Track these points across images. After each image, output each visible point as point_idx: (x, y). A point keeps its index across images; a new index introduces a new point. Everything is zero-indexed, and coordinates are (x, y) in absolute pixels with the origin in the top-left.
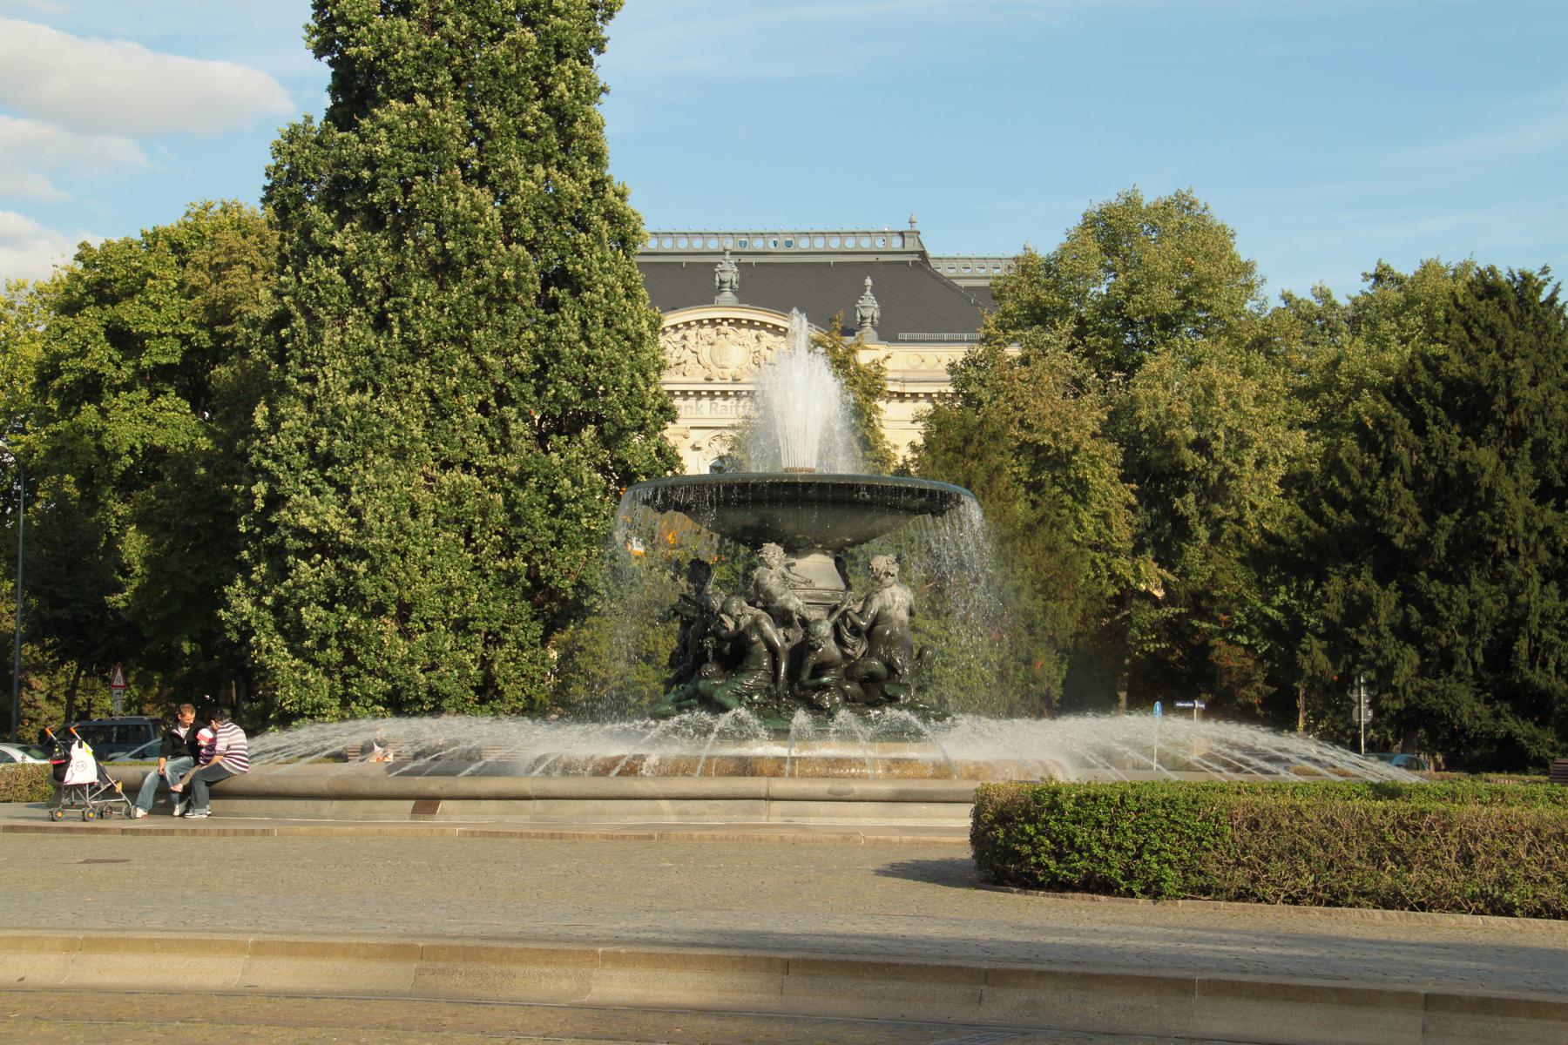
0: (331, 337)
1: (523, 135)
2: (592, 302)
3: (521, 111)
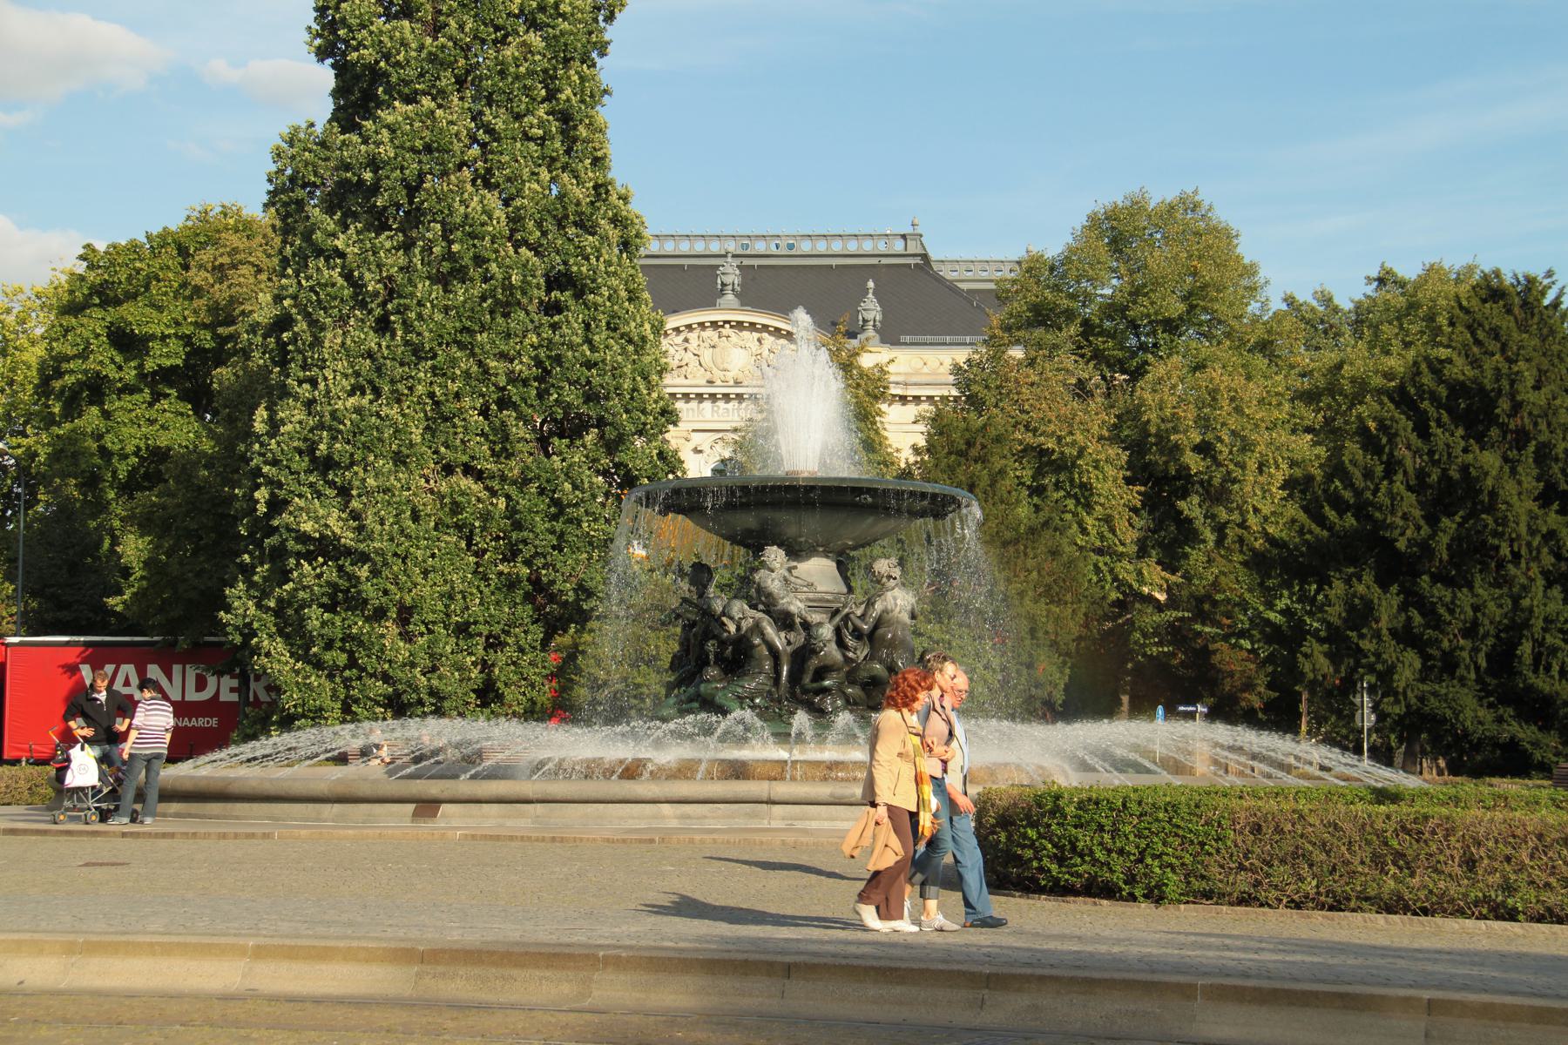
0: (332, 339)
1: (527, 137)
2: (596, 306)
3: (528, 112)
